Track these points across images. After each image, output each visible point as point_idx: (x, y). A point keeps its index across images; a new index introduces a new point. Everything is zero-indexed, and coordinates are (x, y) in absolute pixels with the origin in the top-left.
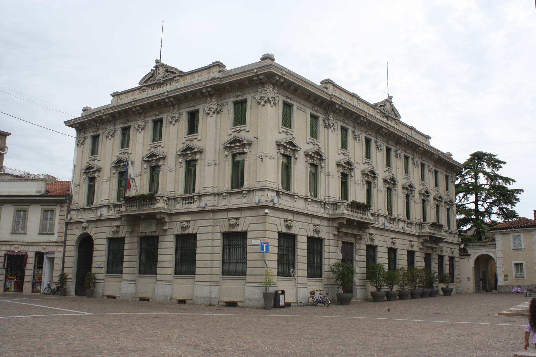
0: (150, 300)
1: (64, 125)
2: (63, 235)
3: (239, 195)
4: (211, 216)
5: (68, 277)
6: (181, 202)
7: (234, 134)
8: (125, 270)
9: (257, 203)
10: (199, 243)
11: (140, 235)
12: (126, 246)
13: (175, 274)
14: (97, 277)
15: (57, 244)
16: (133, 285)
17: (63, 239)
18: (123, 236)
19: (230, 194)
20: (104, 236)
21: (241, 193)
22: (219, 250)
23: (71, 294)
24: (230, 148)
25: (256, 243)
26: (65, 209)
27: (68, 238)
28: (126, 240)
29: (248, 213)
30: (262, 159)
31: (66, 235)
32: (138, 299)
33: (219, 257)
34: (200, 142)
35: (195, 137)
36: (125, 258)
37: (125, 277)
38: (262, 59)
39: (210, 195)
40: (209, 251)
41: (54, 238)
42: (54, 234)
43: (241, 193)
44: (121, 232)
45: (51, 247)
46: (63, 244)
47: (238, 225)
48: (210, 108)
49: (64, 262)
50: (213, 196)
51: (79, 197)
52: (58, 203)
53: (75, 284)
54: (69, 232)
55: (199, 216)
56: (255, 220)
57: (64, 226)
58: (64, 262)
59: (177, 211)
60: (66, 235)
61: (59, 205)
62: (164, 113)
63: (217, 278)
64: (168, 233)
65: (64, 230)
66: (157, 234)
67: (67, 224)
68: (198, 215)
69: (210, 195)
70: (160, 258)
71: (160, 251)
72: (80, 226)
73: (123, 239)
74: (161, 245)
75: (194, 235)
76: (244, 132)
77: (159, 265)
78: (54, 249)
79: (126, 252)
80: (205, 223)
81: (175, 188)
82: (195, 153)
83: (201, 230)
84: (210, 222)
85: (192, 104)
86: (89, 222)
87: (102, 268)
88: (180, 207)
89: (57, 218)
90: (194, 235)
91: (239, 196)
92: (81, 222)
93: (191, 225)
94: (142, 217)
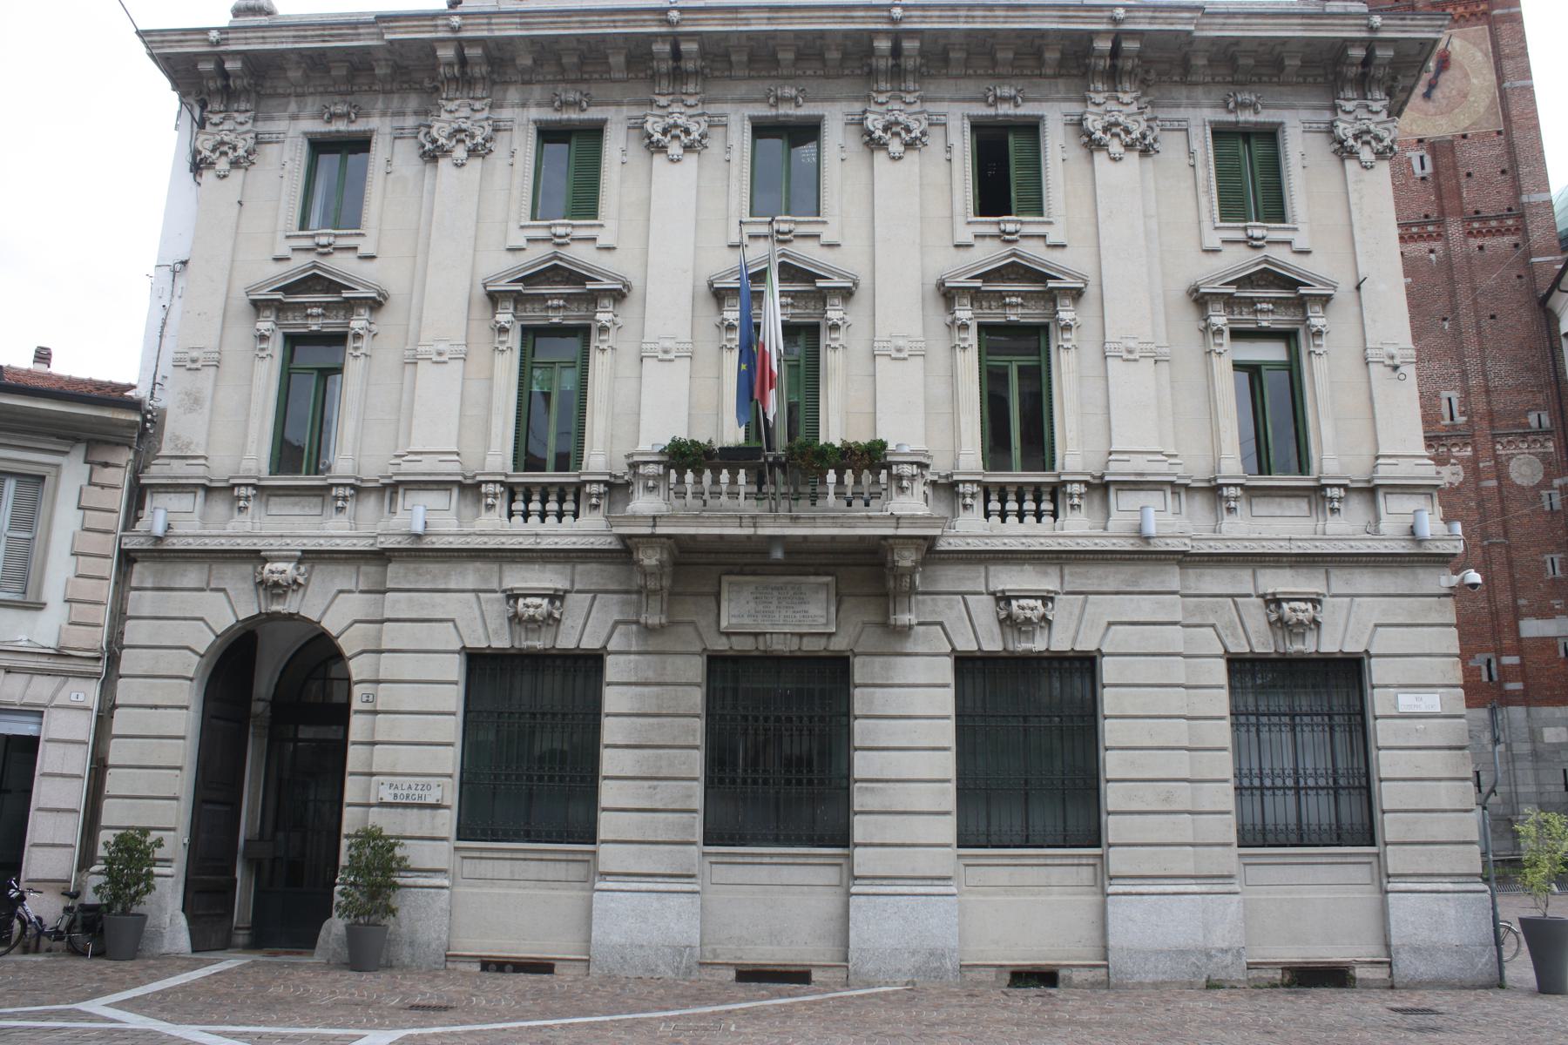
0: (816, 975)
1: (141, 49)
2: (103, 615)
3: (1292, 502)
4: (1172, 578)
5: (158, 853)
6: (501, 505)
7: (301, 261)
8: (607, 825)
9: (159, 539)
10: (1110, 701)
11: (721, 645)
12: (613, 699)
13: (962, 843)
14: (417, 854)
15: (60, 661)
16: (684, 899)
17: (98, 638)
18: (590, 643)
19: (264, 492)
20: (446, 637)
21: (322, 491)
22: (1222, 733)
23: (166, 948)
24: (280, 308)
25: (1423, 709)
26: (119, 477)
27: (134, 632)
28: (614, 668)
29: (1364, 581)
30: (1396, 368)
31: (119, 616)
32: (732, 974)
33: (1224, 765)
34: (367, 265)
35: (341, 242)
36: (610, 761)
37: (609, 857)
38: (237, 12)
39: (1157, 486)
40: (1166, 733)
41: (43, 630)
42: (39, 606)
43: (322, 491)
44: (567, 623)
45: (18, 680)
46: (101, 667)
47: (558, 621)
48: (222, 143)
49: (99, 768)
50: (201, 494)
51: (225, 422)
52: (77, 440)
53: (181, 888)
54: (139, 602)
55: (1113, 577)
56: (1401, 610)
57: (109, 567)
58: (99, 768)
59: (961, 545)
60: (119, 616)
61: (79, 453)
62: (832, 99)
63: (946, 860)
64: (910, 647)
65: (106, 591)
66: (839, 644)
67: (127, 559)
68: (1110, 570)
69: (1157, 486)
70: (862, 765)
71: (861, 731)
72: (237, 580)
73: (590, 664)
74: (861, 700)
75: (1086, 664)
76: (351, 255)
77: (860, 800)
78: (40, 690)
79: (611, 730)
80: (1144, 608)
81: (459, 443)
82: (350, 306)
83: (1120, 638)
84: (1174, 608)
85: (789, 91)
86: (310, 557)
87: (436, 806)
88: (972, 527)
89: (65, 520)
90: (1086, 664)
91: (311, 506)
92: (256, 557)
93: (1062, 613)
94: (778, 554)
